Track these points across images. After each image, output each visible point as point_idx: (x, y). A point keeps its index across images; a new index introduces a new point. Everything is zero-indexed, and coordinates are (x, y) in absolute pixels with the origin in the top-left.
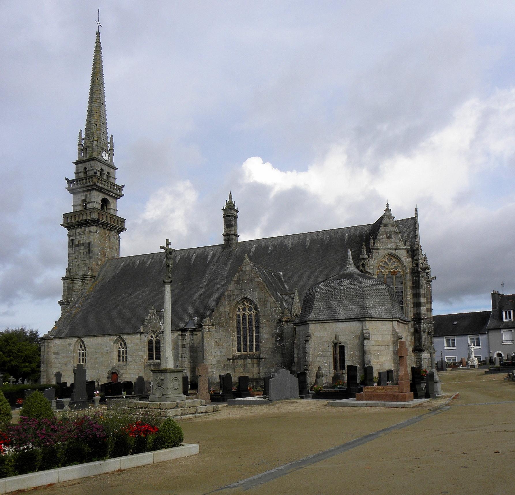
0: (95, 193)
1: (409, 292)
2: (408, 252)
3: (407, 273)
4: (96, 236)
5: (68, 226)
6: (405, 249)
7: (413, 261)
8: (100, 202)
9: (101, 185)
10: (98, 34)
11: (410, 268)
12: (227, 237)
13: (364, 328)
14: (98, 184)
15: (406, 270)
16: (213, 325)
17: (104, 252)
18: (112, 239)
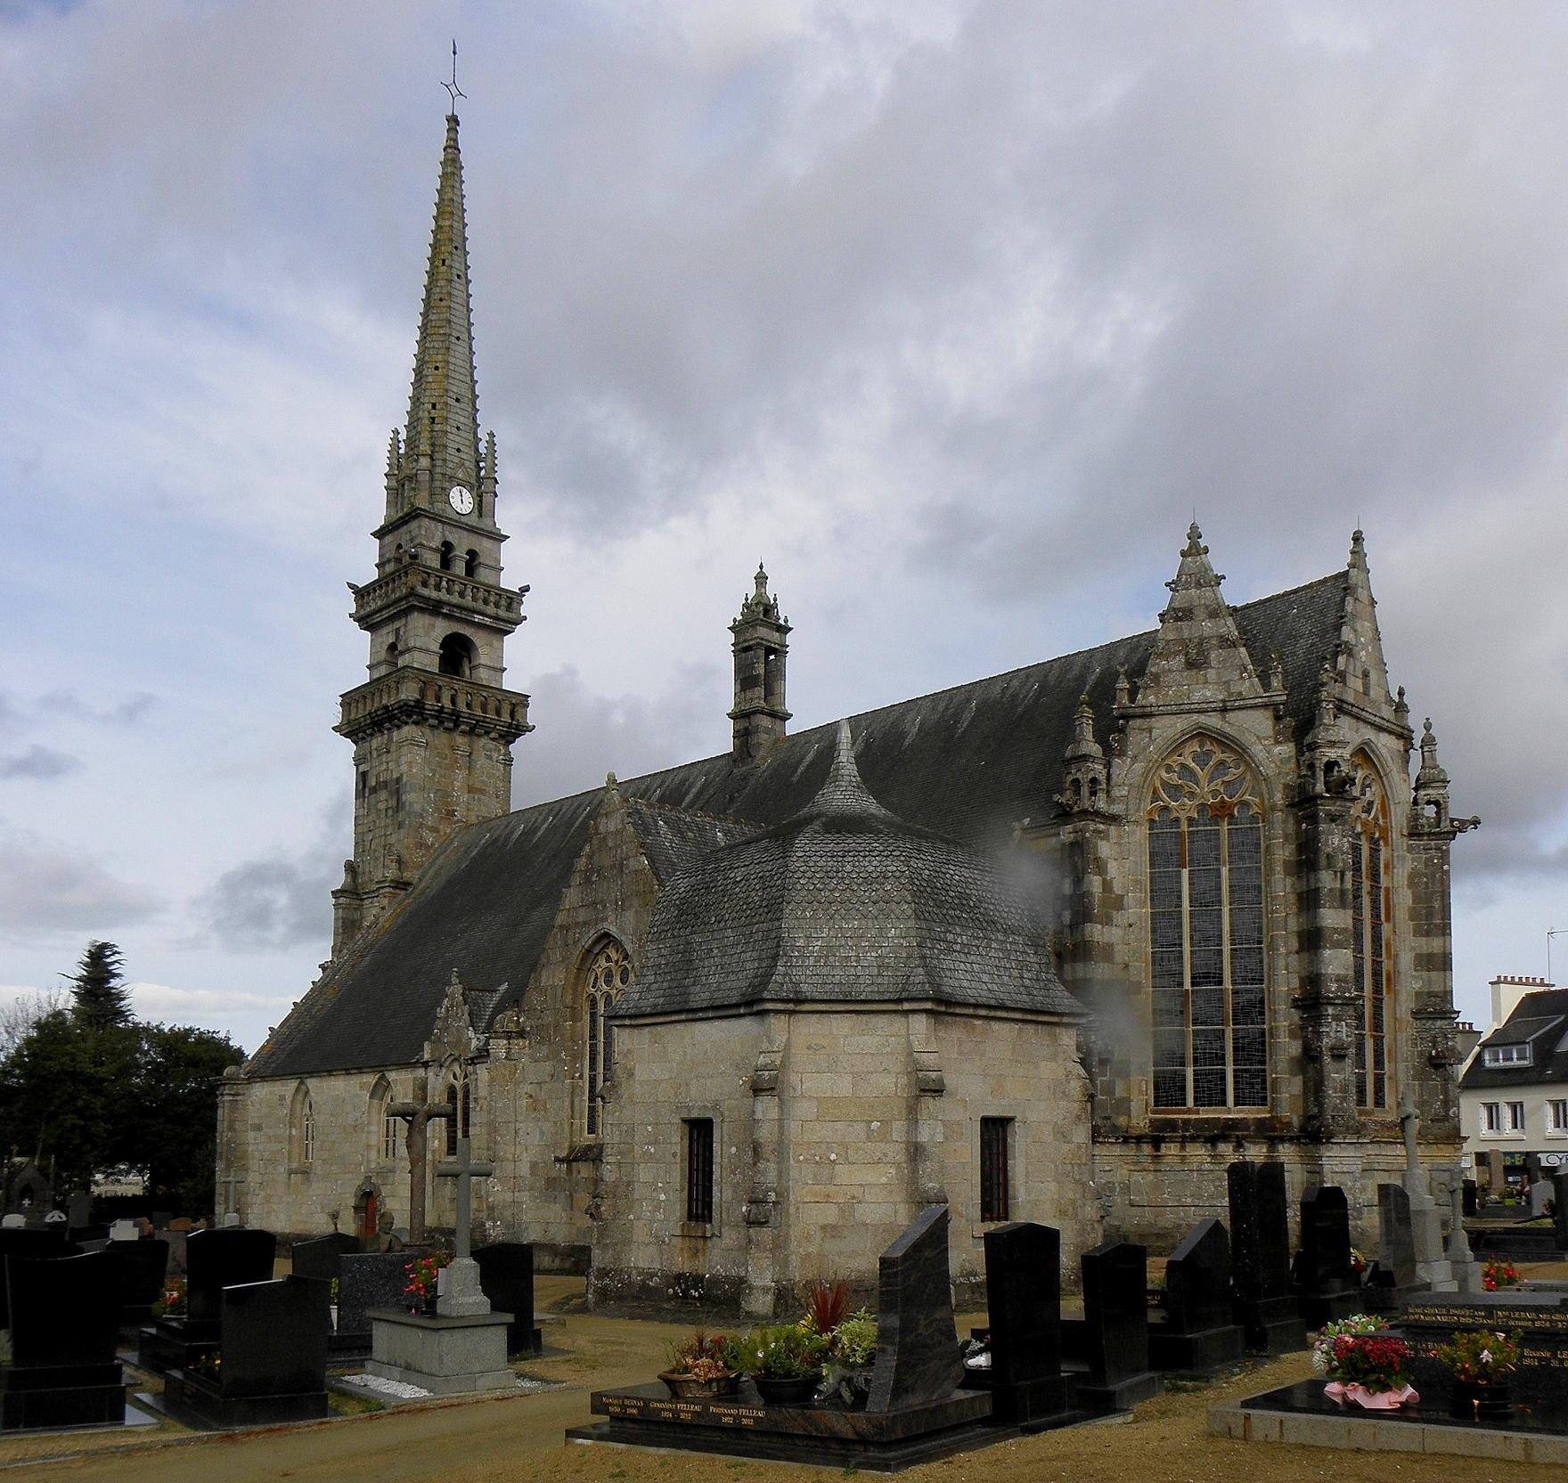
0: (418, 621)
1: (1280, 886)
2: (1278, 718)
3: (1273, 808)
4: (418, 755)
5: (350, 730)
6: (1265, 706)
7: (1300, 752)
8: (435, 647)
9: (434, 594)
10: (453, 121)
11: (1286, 786)
12: (744, 723)
14: (425, 592)
15: (1271, 796)
16: (521, 1034)
17: (448, 804)
18: (481, 762)
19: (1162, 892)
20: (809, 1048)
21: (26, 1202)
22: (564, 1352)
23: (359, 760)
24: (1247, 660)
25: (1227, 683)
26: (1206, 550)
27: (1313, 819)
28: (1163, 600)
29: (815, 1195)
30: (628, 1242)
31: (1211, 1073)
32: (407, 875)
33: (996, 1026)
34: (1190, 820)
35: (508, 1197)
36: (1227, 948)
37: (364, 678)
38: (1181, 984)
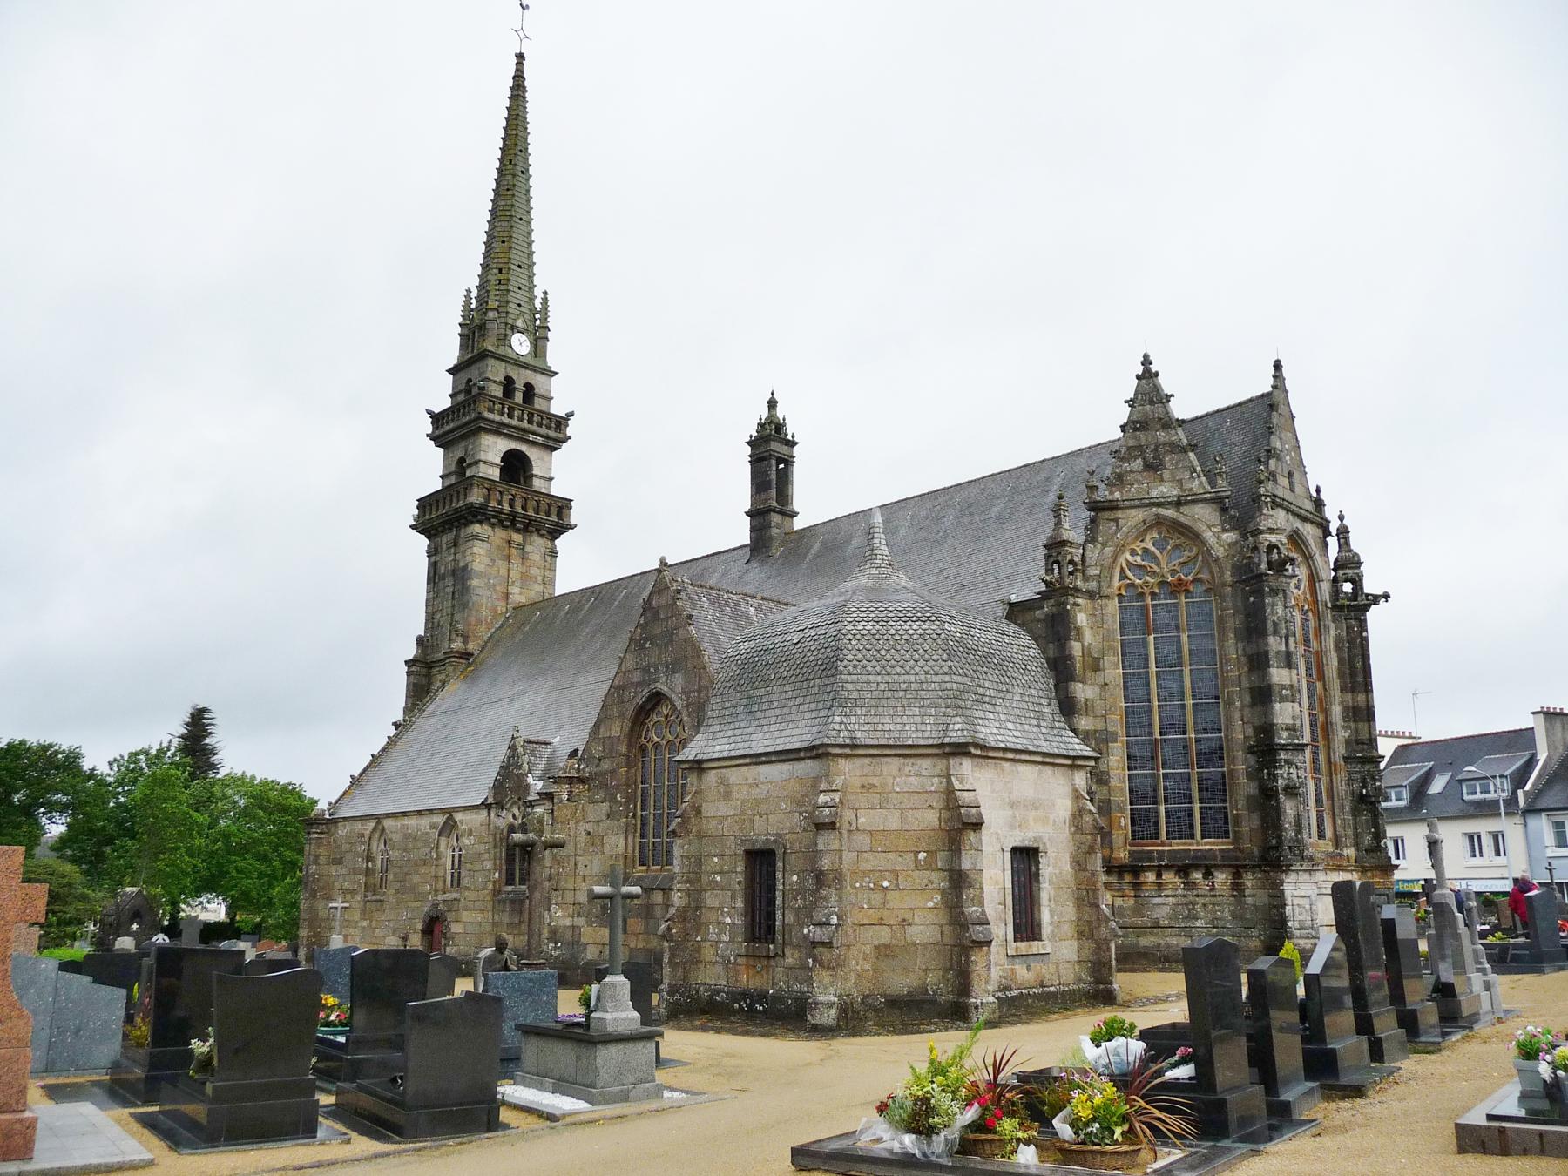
2: (1224, 510)
3: (1224, 585)
5: (421, 526)
8: (498, 461)
9: (497, 418)
10: (520, 57)
13: (957, 785)
15: (1222, 573)
16: (581, 780)
19: (1133, 656)
20: (863, 787)
21: (135, 926)
22: (686, 1064)
23: (432, 552)
24: (1196, 463)
25: (1180, 481)
26: (1157, 374)
27: (1259, 593)
28: (1123, 414)
29: (869, 917)
30: (697, 962)
31: (1180, 810)
32: (471, 647)
33: (1021, 768)
34: (1153, 594)
35: (568, 922)
36: (1189, 702)
37: (437, 485)
38: (1151, 734)
